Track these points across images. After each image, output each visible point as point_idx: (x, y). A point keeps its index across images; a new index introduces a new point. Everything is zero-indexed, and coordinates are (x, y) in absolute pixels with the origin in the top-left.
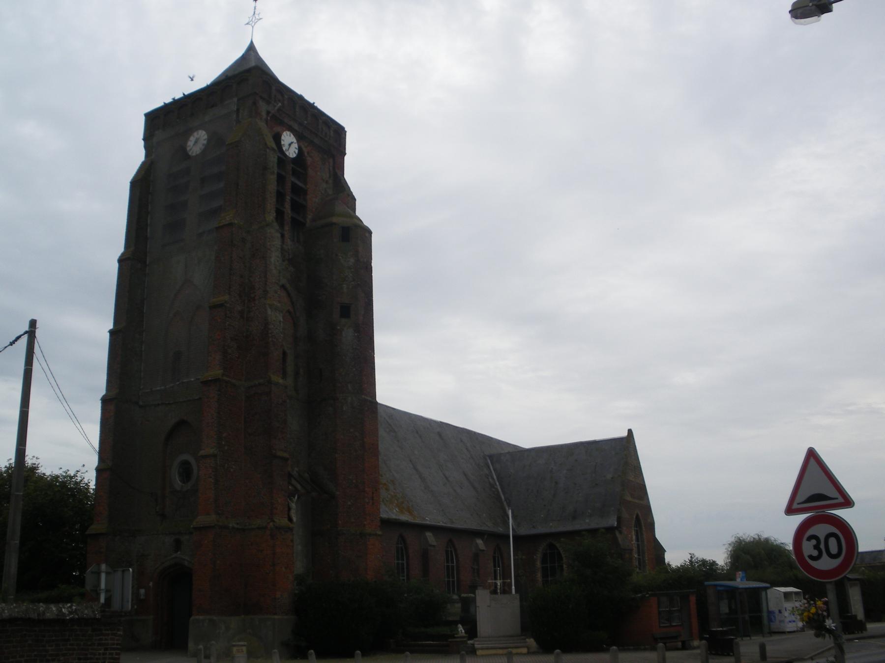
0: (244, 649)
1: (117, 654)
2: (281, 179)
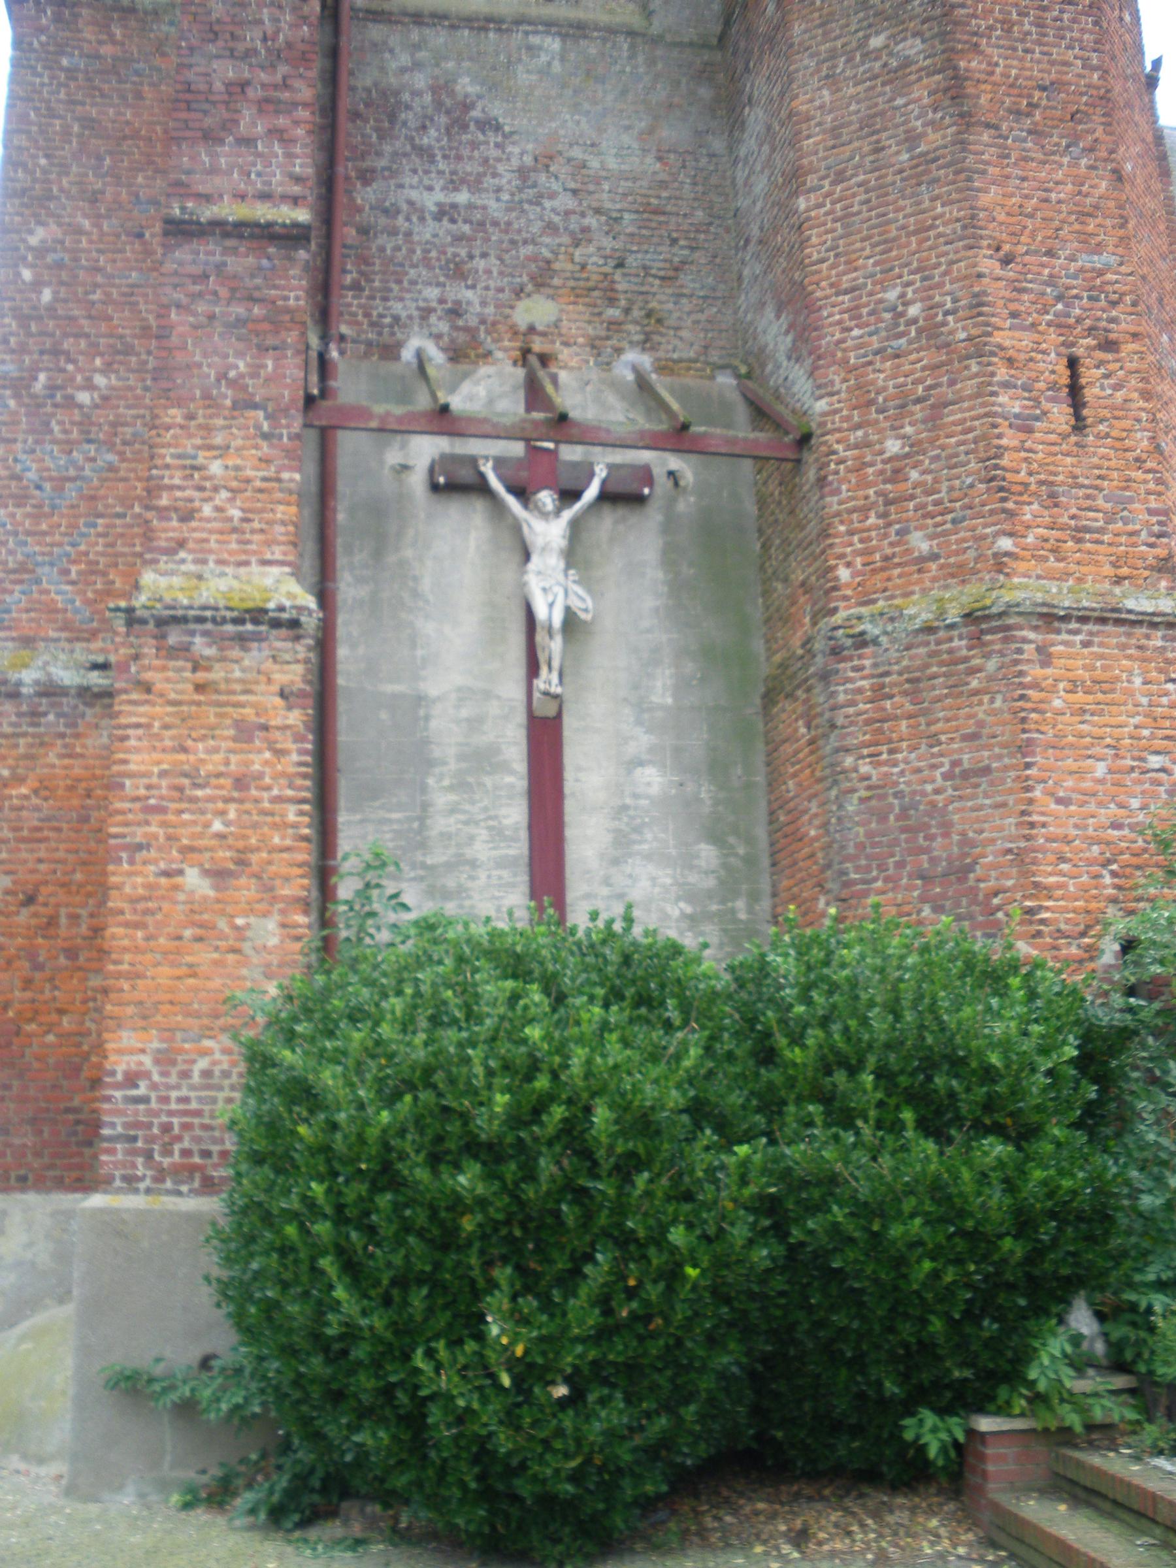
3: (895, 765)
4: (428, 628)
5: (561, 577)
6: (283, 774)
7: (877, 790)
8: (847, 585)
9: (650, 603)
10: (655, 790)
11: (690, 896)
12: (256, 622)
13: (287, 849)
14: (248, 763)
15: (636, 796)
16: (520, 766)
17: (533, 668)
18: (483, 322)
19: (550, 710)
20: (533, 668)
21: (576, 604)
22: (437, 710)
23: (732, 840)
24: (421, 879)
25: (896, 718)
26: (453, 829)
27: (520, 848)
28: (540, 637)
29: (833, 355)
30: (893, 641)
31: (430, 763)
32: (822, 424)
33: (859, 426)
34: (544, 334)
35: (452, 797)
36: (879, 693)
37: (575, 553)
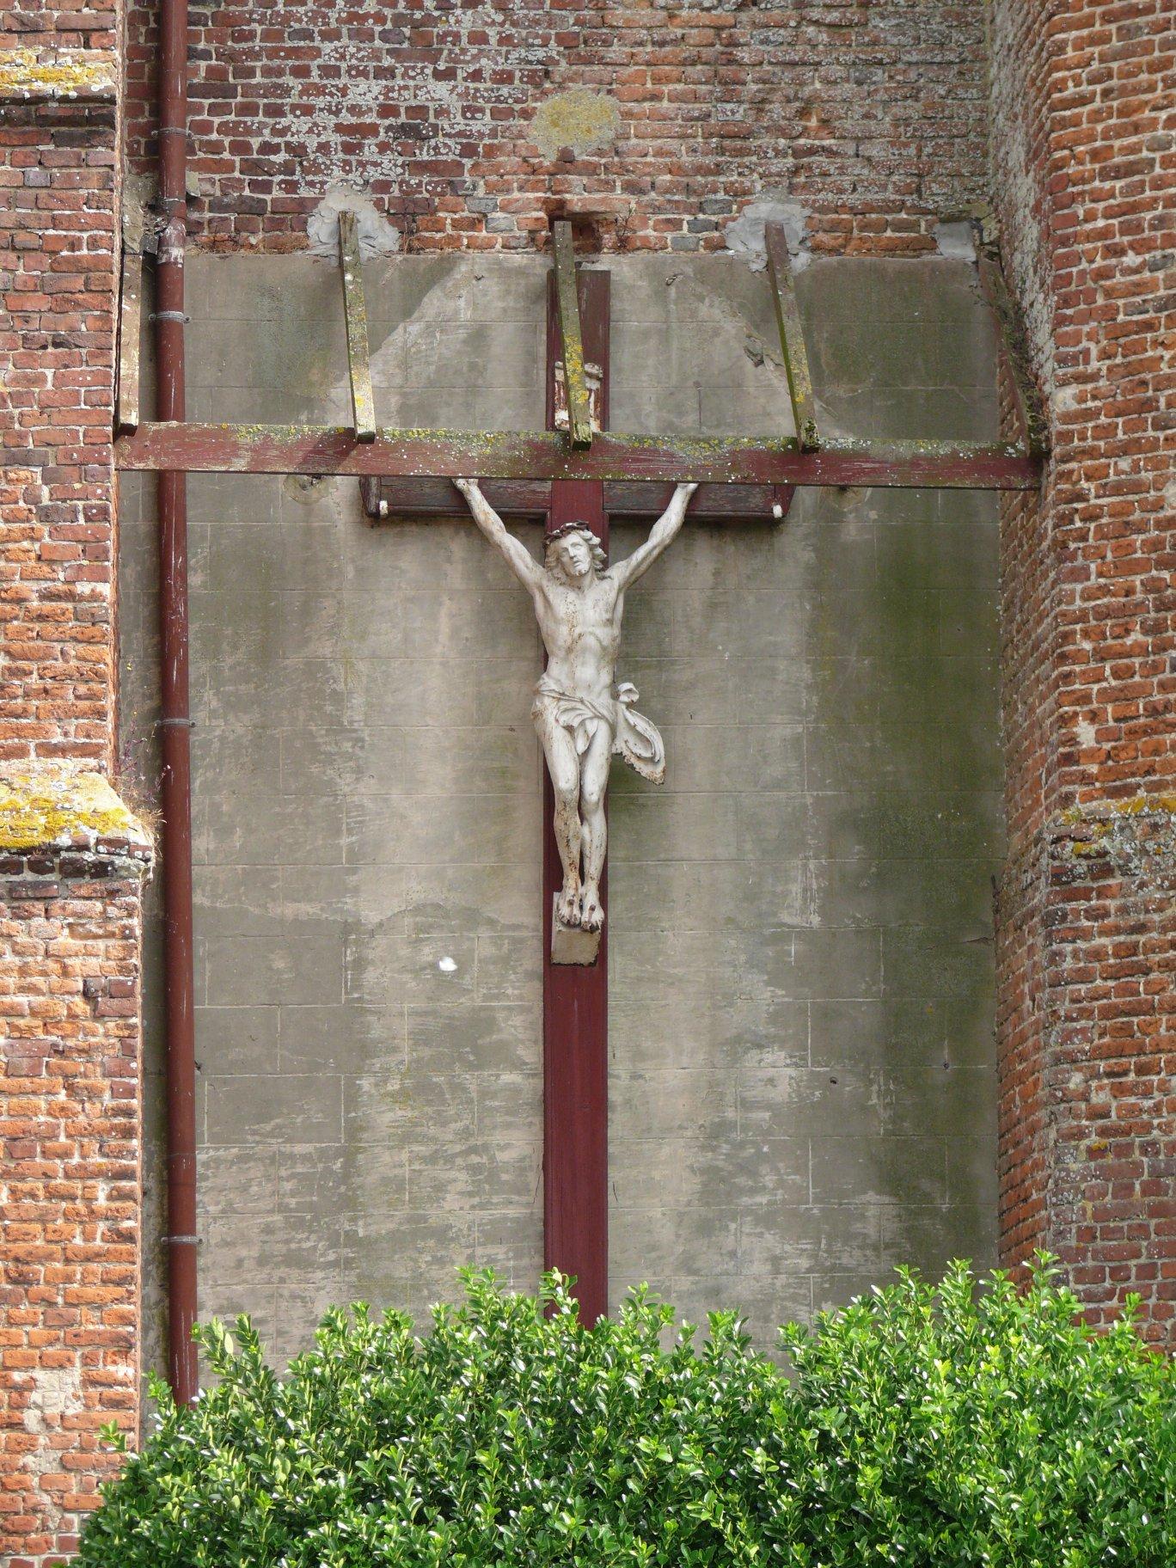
3: (1147, 1094)
4: (361, 792)
5: (603, 701)
6: (91, 1132)
7: (1119, 1137)
8: (1091, 755)
9: (783, 729)
10: (781, 1093)
12: (38, 868)
13: (97, 1256)
14: (26, 1113)
15: (745, 1105)
16: (532, 1054)
17: (553, 878)
18: (469, 150)
19: (584, 952)
20: (553, 878)
21: (629, 746)
22: (378, 948)
23: (926, 1185)
24: (348, 1264)
25: (1151, 1009)
26: (406, 1172)
27: (522, 1206)
28: (567, 822)
29: (1090, 297)
30: (1155, 869)
31: (366, 1051)
32: (1066, 437)
33: (1124, 450)
34: (590, 170)
35: (401, 1113)
37: (638, 645)
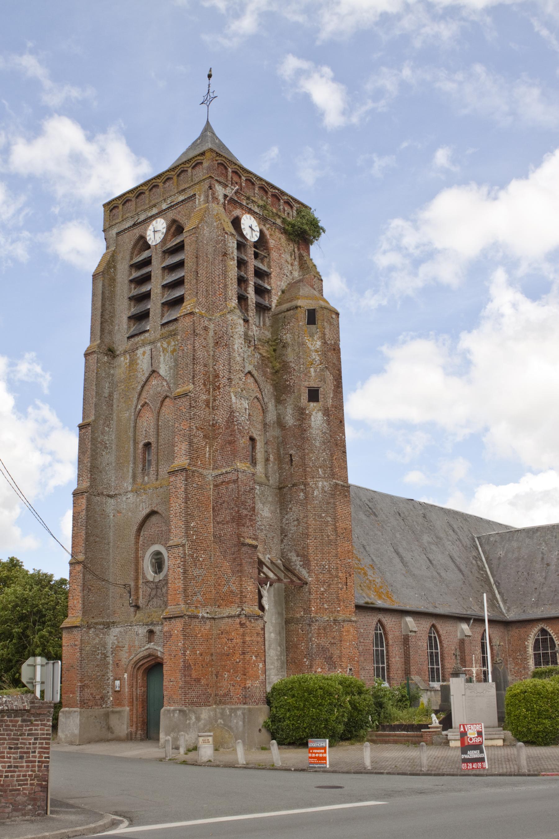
0: (211, 739)
1: (47, 744)
2: (241, 263)
7: (318, 645)
11: (277, 656)
36: (319, 629)
